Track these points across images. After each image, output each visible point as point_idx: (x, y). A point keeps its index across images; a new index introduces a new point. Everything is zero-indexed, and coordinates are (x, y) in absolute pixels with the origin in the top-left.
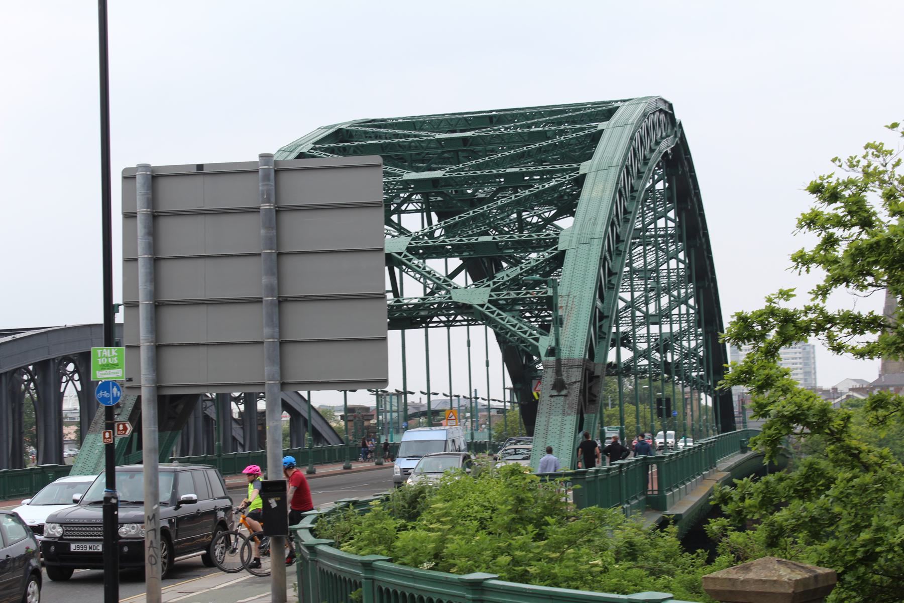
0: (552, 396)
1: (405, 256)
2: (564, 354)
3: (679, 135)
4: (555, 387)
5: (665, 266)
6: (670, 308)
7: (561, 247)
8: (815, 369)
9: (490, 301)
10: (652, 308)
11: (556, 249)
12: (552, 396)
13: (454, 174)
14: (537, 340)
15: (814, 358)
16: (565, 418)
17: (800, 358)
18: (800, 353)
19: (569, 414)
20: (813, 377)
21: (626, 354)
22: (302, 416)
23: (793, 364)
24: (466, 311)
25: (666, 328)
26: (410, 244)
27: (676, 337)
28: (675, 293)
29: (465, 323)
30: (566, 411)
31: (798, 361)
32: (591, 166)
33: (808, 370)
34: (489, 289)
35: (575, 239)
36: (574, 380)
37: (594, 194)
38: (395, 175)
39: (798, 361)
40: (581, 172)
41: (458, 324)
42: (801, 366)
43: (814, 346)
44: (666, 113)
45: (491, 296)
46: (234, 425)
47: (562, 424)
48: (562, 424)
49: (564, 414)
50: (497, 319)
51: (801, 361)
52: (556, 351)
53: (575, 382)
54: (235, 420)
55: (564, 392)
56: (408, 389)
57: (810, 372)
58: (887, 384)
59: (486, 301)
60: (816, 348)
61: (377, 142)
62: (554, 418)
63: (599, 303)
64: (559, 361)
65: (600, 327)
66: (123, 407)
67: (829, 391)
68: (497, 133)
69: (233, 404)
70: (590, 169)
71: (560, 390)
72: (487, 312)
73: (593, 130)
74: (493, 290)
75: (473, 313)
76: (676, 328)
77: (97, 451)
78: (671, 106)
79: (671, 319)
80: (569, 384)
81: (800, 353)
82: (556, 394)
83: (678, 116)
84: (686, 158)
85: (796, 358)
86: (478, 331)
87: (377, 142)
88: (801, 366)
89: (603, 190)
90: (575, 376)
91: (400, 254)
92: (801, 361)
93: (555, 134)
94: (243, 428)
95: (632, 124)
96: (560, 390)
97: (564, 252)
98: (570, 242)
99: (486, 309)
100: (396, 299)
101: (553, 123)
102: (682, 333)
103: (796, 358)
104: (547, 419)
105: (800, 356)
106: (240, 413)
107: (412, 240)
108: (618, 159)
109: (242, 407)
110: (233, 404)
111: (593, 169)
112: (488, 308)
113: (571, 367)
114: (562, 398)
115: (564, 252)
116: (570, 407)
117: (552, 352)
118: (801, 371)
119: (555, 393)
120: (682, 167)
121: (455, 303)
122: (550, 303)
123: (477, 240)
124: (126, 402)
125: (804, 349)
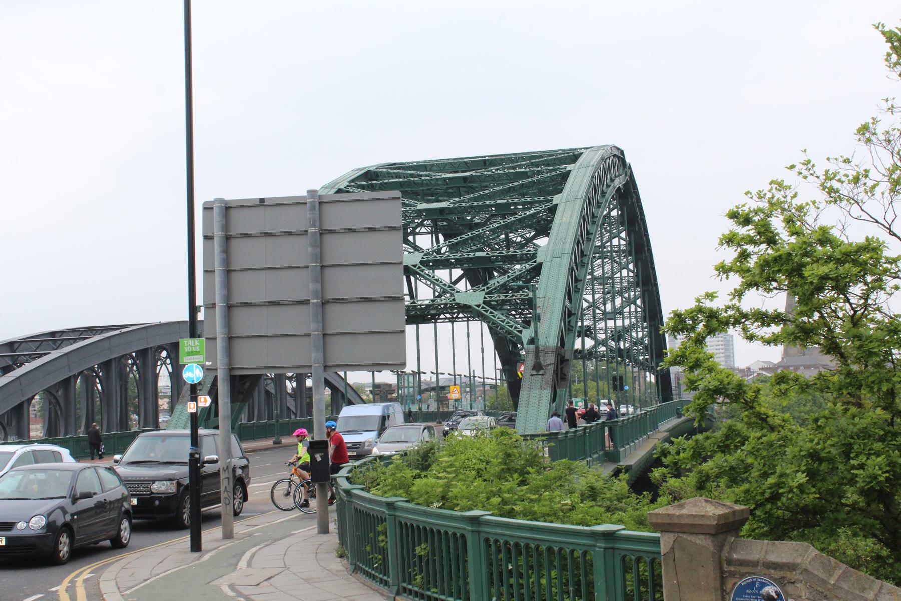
0: (532, 375)
1: (419, 268)
2: (541, 343)
3: (629, 174)
4: (534, 368)
5: (618, 275)
6: (623, 307)
7: (538, 260)
8: (733, 353)
9: (484, 302)
10: (609, 307)
11: (535, 262)
12: (532, 375)
13: (456, 205)
14: (520, 332)
15: (733, 345)
16: (542, 392)
17: (722, 345)
18: (722, 341)
19: (545, 389)
20: (732, 359)
21: (589, 343)
22: (341, 391)
23: (717, 349)
24: (466, 310)
25: (619, 323)
26: (423, 258)
27: (627, 330)
28: (626, 295)
29: (466, 319)
30: (543, 385)
31: (721, 347)
32: (562, 198)
33: (728, 354)
34: (483, 293)
35: (549, 255)
36: (549, 363)
37: (564, 219)
38: (411, 206)
39: (721, 347)
40: (554, 203)
41: (460, 319)
42: (723, 351)
43: (732, 336)
44: (618, 157)
45: (485, 298)
46: (289, 398)
47: (540, 396)
48: (540, 396)
49: (541, 389)
50: (490, 315)
51: (723, 347)
52: (535, 340)
53: (550, 364)
54: (289, 394)
55: (541, 372)
56: (422, 370)
57: (730, 356)
58: (788, 364)
59: (482, 302)
60: (734, 337)
61: (397, 180)
62: (534, 392)
63: (568, 303)
64: (537, 348)
65: (569, 322)
66: (204, 384)
67: (744, 370)
68: (489, 173)
69: (288, 382)
70: (561, 200)
71: (538, 371)
72: (482, 311)
73: (563, 171)
74: (486, 294)
75: (471, 311)
76: (627, 322)
77: (184, 418)
78: (622, 152)
79: (623, 315)
80: (545, 366)
81: (722, 341)
82: (535, 373)
83: (628, 160)
84: (634, 192)
85: (719, 345)
86: (475, 325)
87: (397, 180)
88: (723, 351)
89: (571, 217)
90: (549, 360)
91: (415, 266)
92: (723, 347)
93: (534, 174)
94: (295, 400)
95: (593, 166)
96: (538, 371)
97: (541, 264)
98: (546, 257)
99: (481, 308)
100: (412, 301)
101: (532, 165)
102: (632, 326)
103: (719, 345)
104: (528, 392)
105: (722, 343)
106: (293, 389)
107: (424, 255)
108: (582, 193)
109: (294, 384)
110: (288, 382)
111: (563, 201)
112: (483, 307)
113: (546, 353)
114: (540, 376)
115: (541, 264)
116: (546, 383)
117: (532, 341)
118: (723, 355)
119: (534, 372)
120: (632, 199)
121: (458, 304)
122: (530, 303)
123: (474, 255)
124: (206, 380)
125: (725, 338)
